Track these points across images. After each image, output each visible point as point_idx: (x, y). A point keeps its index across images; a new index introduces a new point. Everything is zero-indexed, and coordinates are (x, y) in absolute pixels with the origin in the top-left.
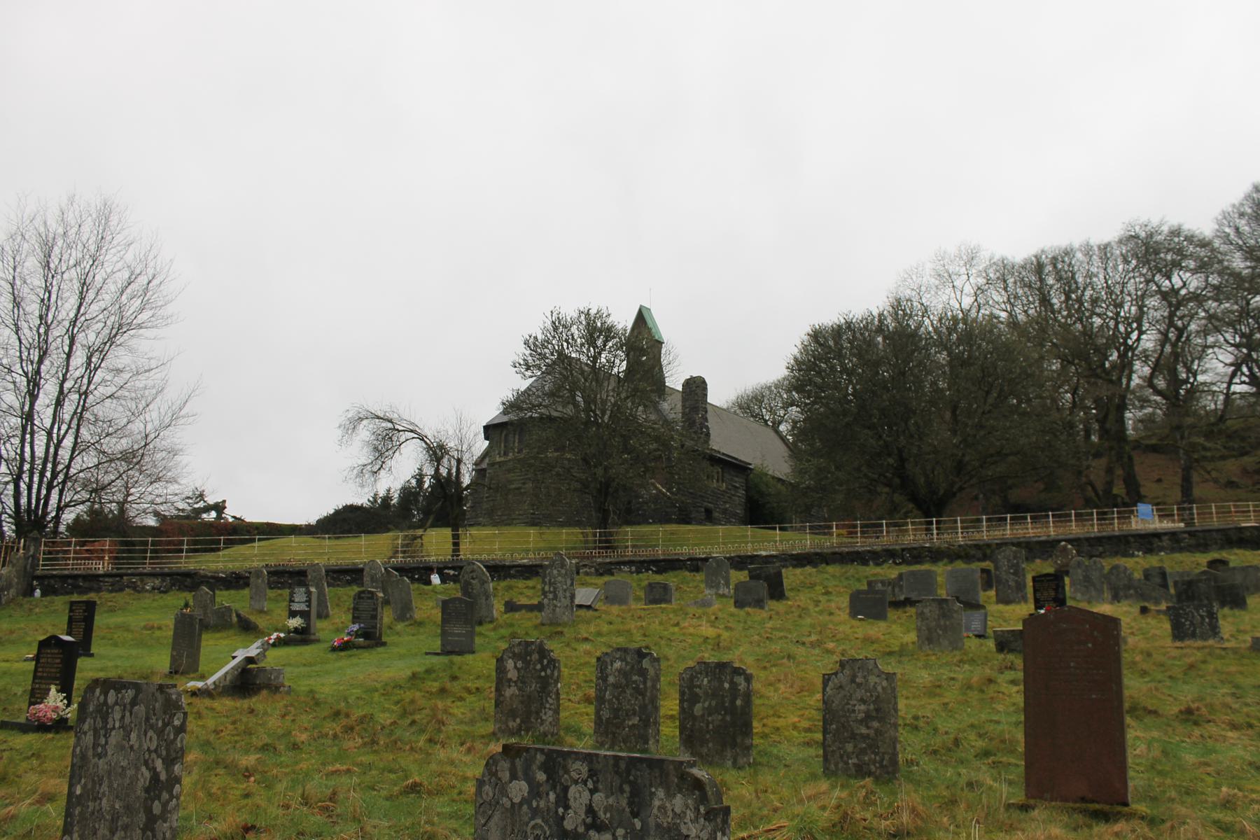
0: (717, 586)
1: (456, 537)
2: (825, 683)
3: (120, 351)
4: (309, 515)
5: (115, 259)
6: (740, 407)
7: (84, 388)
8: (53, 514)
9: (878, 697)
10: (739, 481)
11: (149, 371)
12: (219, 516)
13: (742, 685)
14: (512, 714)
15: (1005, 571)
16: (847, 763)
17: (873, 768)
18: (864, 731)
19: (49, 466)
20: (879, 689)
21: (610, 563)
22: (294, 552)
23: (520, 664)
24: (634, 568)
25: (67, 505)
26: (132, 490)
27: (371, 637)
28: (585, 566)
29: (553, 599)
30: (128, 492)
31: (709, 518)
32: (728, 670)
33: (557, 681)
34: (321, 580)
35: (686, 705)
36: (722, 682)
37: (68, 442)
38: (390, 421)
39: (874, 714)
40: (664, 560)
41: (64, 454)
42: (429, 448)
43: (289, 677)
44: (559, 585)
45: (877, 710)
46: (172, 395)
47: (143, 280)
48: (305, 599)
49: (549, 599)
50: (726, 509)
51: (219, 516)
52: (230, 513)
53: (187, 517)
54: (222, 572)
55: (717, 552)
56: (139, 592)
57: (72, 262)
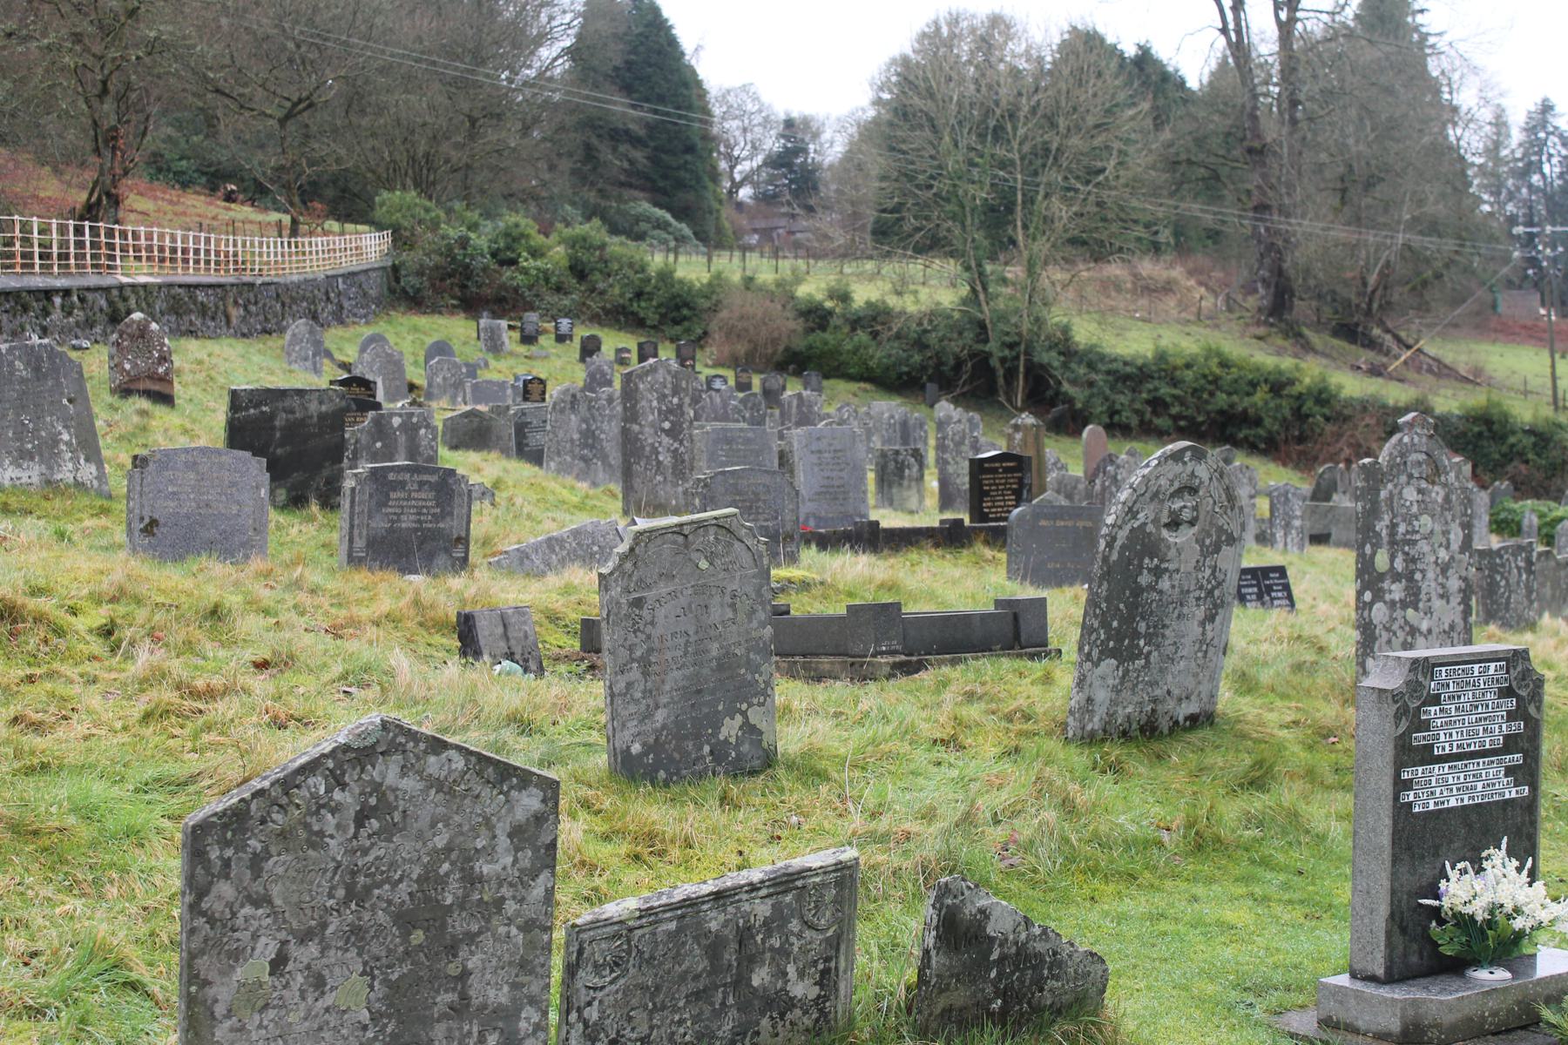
0: (48, 452)
15: (652, 425)
29: (1404, 605)
44: (1424, 546)
48: (1501, 729)
49: (1392, 604)
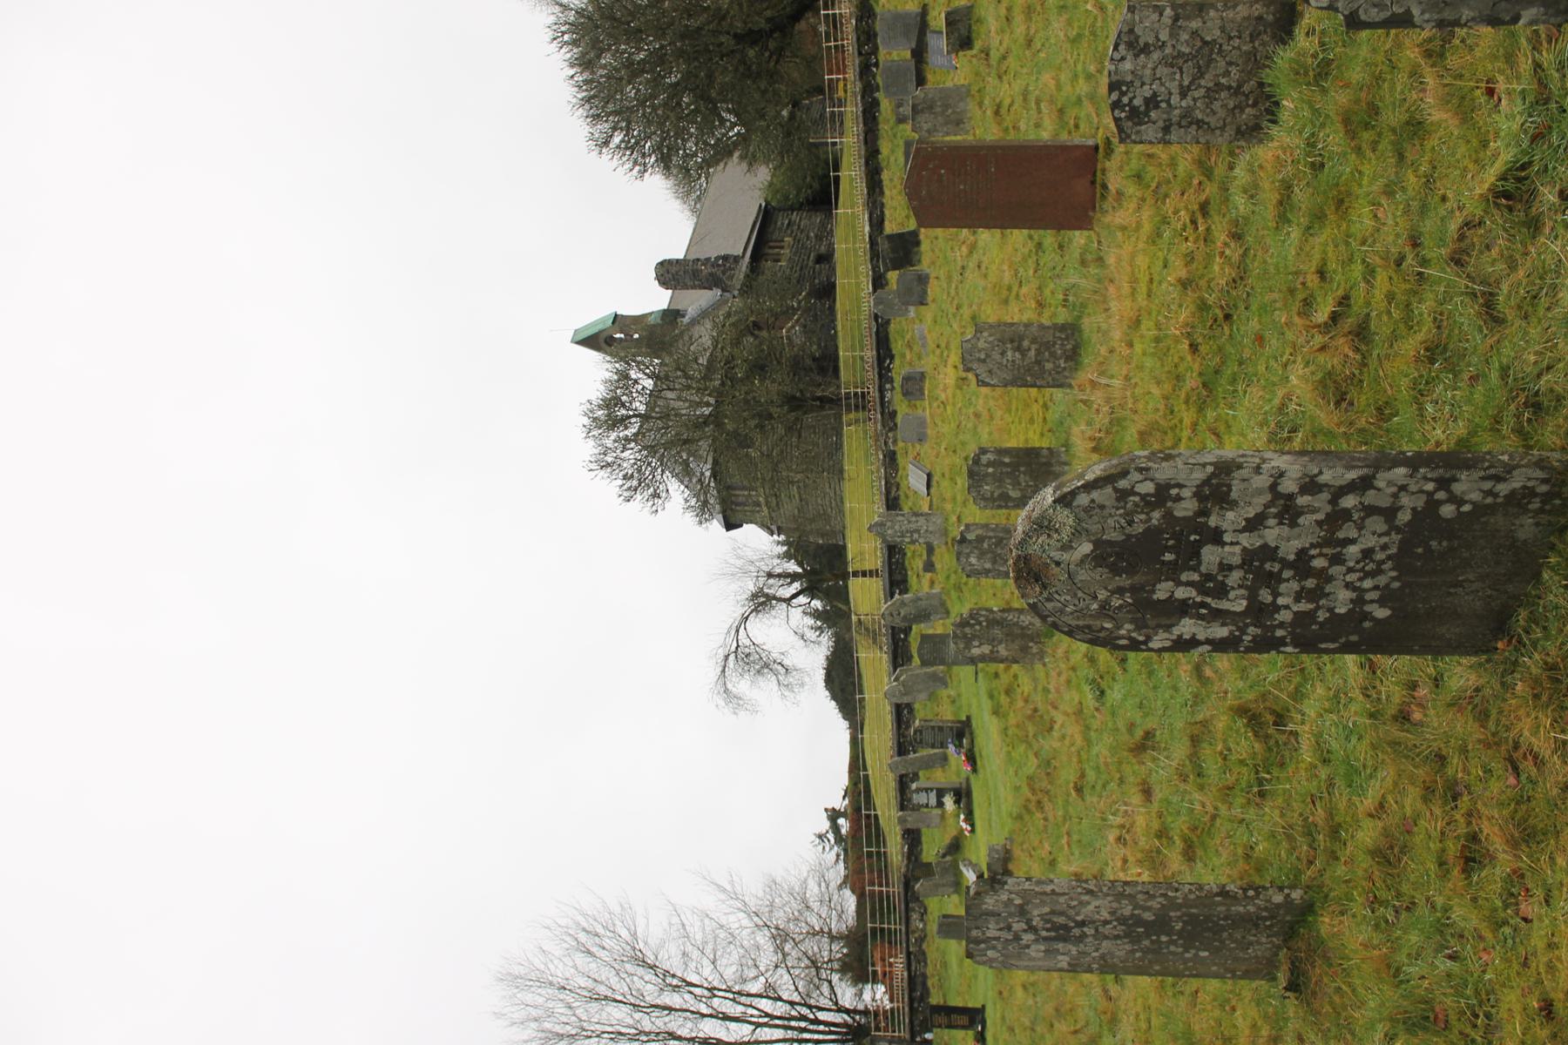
1: (855, 574)
2: (986, 384)
3: (663, 955)
4: (840, 730)
5: (561, 966)
6: (688, 194)
7: (706, 993)
8: (846, 1017)
9: (999, 340)
10: (782, 221)
11: (683, 925)
12: (844, 815)
13: (990, 456)
14: (1025, 649)
16: (1065, 368)
17: (1069, 347)
18: (1032, 353)
19: (793, 1023)
20: (991, 339)
21: (882, 414)
22: (880, 736)
23: (976, 643)
24: (888, 386)
25: (836, 1003)
26: (817, 928)
27: (962, 731)
28: (886, 443)
30: (818, 933)
31: (826, 258)
32: (976, 468)
33: (990, 611)
34: (906, 761)
35: (1010, 504)
36: (987, 474)
37: (765, 1004)
38: (727, 657)
39: (1016, 344)
40: (878, 351)
41: (780, 1009)
42: (756, 610)
43: (998, 840)
45: (1012, 341)
46: (709, 900)
47: (582, 937)
50: (816, 236)
51: (844, 815)
52: (839, 803)
53: (845, 850)
54: (903, 848)
55: (868, 304)
56: (925, 936)
57: (569, 1012)
